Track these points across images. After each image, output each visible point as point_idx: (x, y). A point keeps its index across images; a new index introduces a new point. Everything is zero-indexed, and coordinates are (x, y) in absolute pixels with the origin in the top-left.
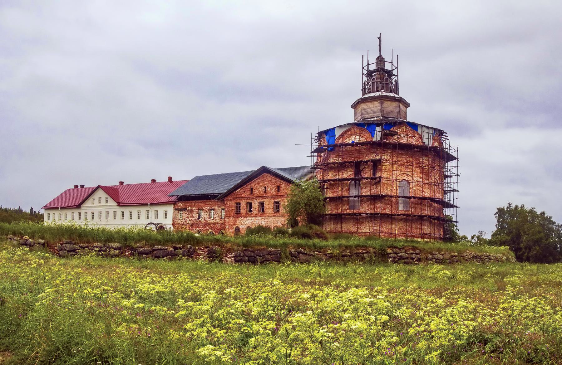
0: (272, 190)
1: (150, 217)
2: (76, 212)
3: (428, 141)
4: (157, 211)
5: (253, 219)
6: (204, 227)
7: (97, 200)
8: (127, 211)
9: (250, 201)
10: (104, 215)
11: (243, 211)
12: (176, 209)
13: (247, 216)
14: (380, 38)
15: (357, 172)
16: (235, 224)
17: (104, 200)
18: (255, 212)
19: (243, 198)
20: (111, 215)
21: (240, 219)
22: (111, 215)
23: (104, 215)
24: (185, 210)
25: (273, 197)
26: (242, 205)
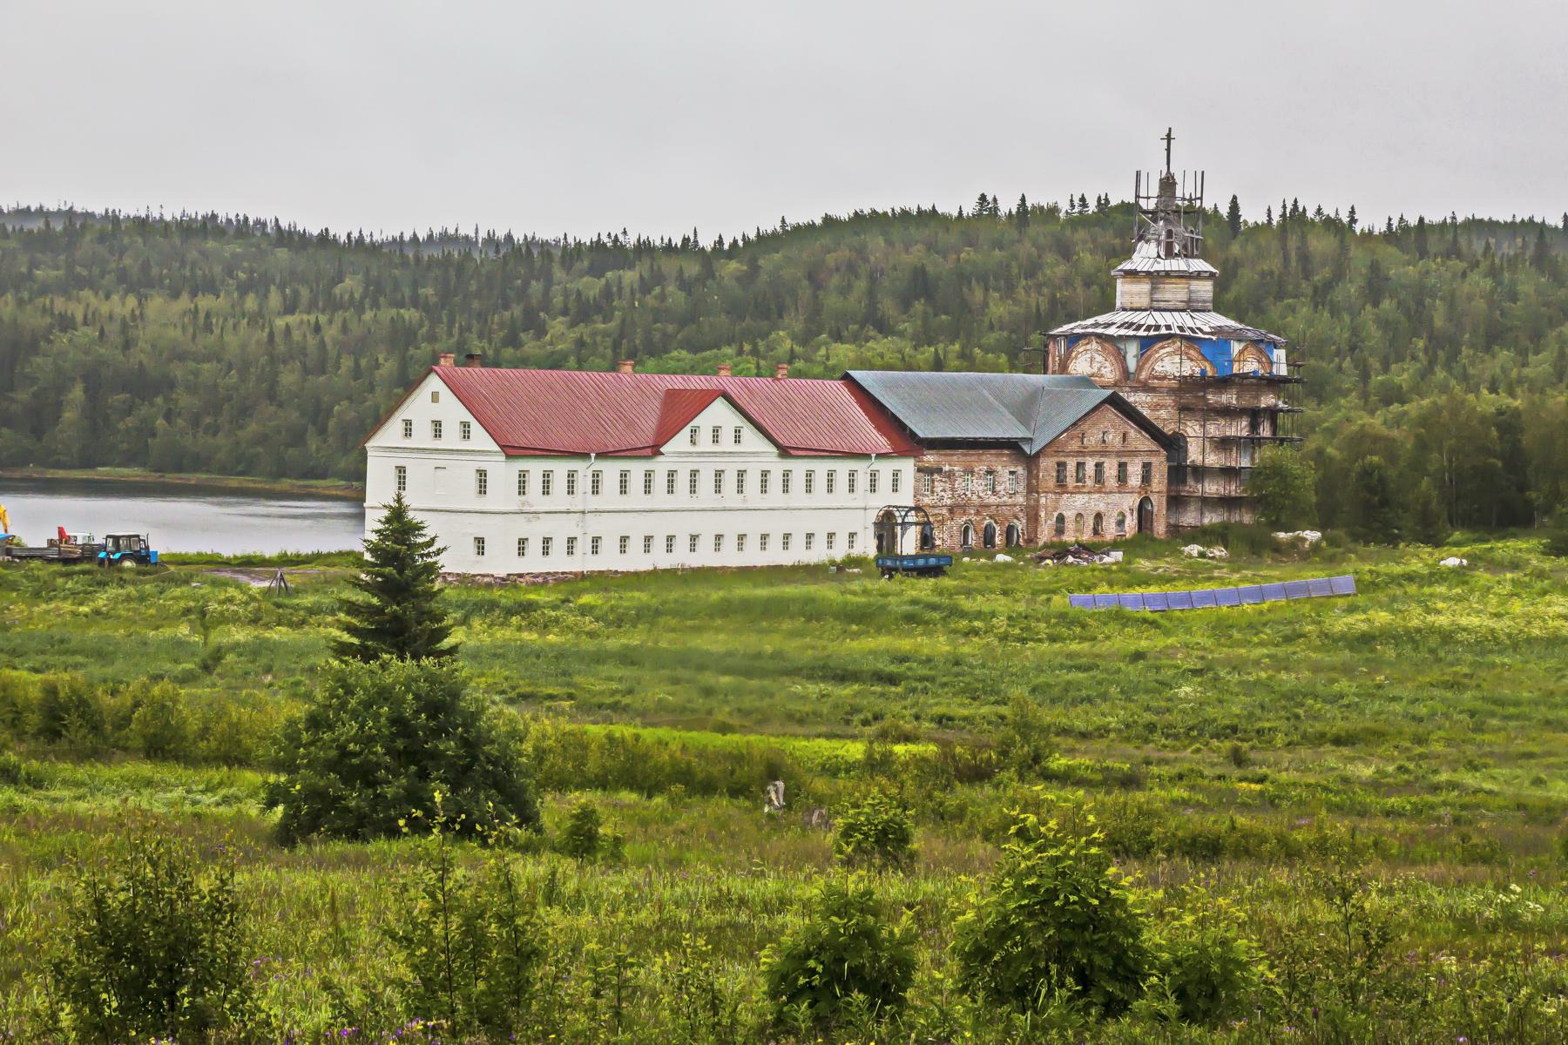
0: (1114, 439)
1: (590, 479)
2: (637, 469)
3: (1163, 331)
4: (624, 475)
5: (1086, 497)
6: (978, 513)
7: (705, 436)
8: (799, 467)
9: (1080, 460)
10: (730, 481)
11: (1071, 482)
12: (919, 470)
13: (1077, 491)
14: (1169, 138)
15: (1254, 427)
16: (1055, 509)
17: (727, 436)
18: (1089, 483)
19: (1069, 454)
20: (752, 481)
21: (1065, 496)
22: (752, 481)
23: (730, 481)
24: (939, 471)
25: (1119, 454)
26: (1130, 469)
